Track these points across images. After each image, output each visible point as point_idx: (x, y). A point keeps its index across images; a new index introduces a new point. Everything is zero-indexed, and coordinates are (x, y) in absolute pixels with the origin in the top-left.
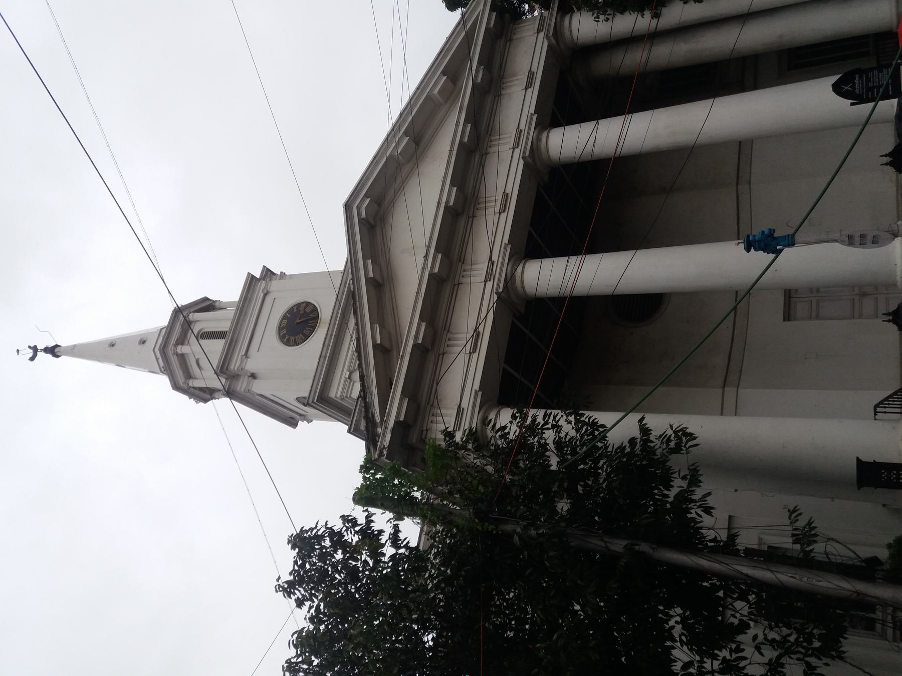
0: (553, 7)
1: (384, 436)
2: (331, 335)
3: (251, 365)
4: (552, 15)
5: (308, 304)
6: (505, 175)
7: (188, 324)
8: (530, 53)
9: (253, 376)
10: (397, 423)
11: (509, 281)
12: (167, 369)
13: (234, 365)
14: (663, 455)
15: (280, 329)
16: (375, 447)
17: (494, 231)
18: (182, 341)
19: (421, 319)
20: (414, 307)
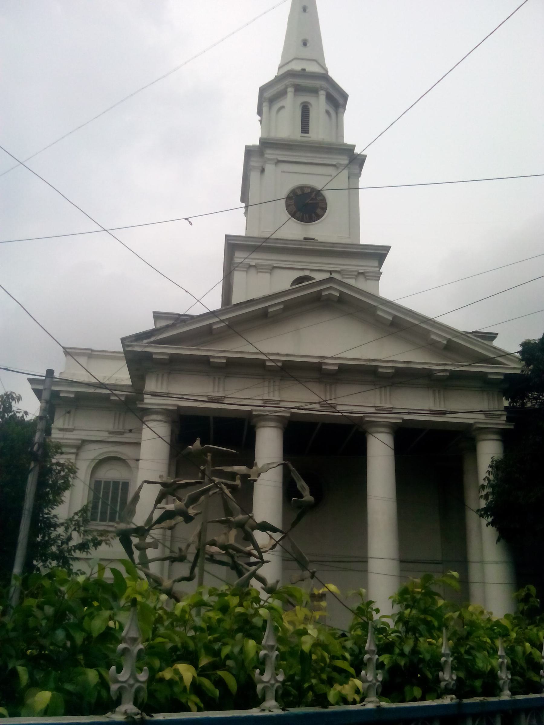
0: (509, 425)
1: (140, 346)
2: (285, 244)
3: (270, 168)
4: (502, 422)
5: (324, 209)
6: (352, 402)
7: (314, 91)
8: (464, 409)
9: (263, 171)
10: (151, 354)
11: (262, 418)
12: (278, 79)
13: (270, 154)
14: (491, 517)
15: (302, 188)
16: (131, 342)
17: (302, 399)
18: (299, 89)
19: (228, 358)
20: (237, 352)
